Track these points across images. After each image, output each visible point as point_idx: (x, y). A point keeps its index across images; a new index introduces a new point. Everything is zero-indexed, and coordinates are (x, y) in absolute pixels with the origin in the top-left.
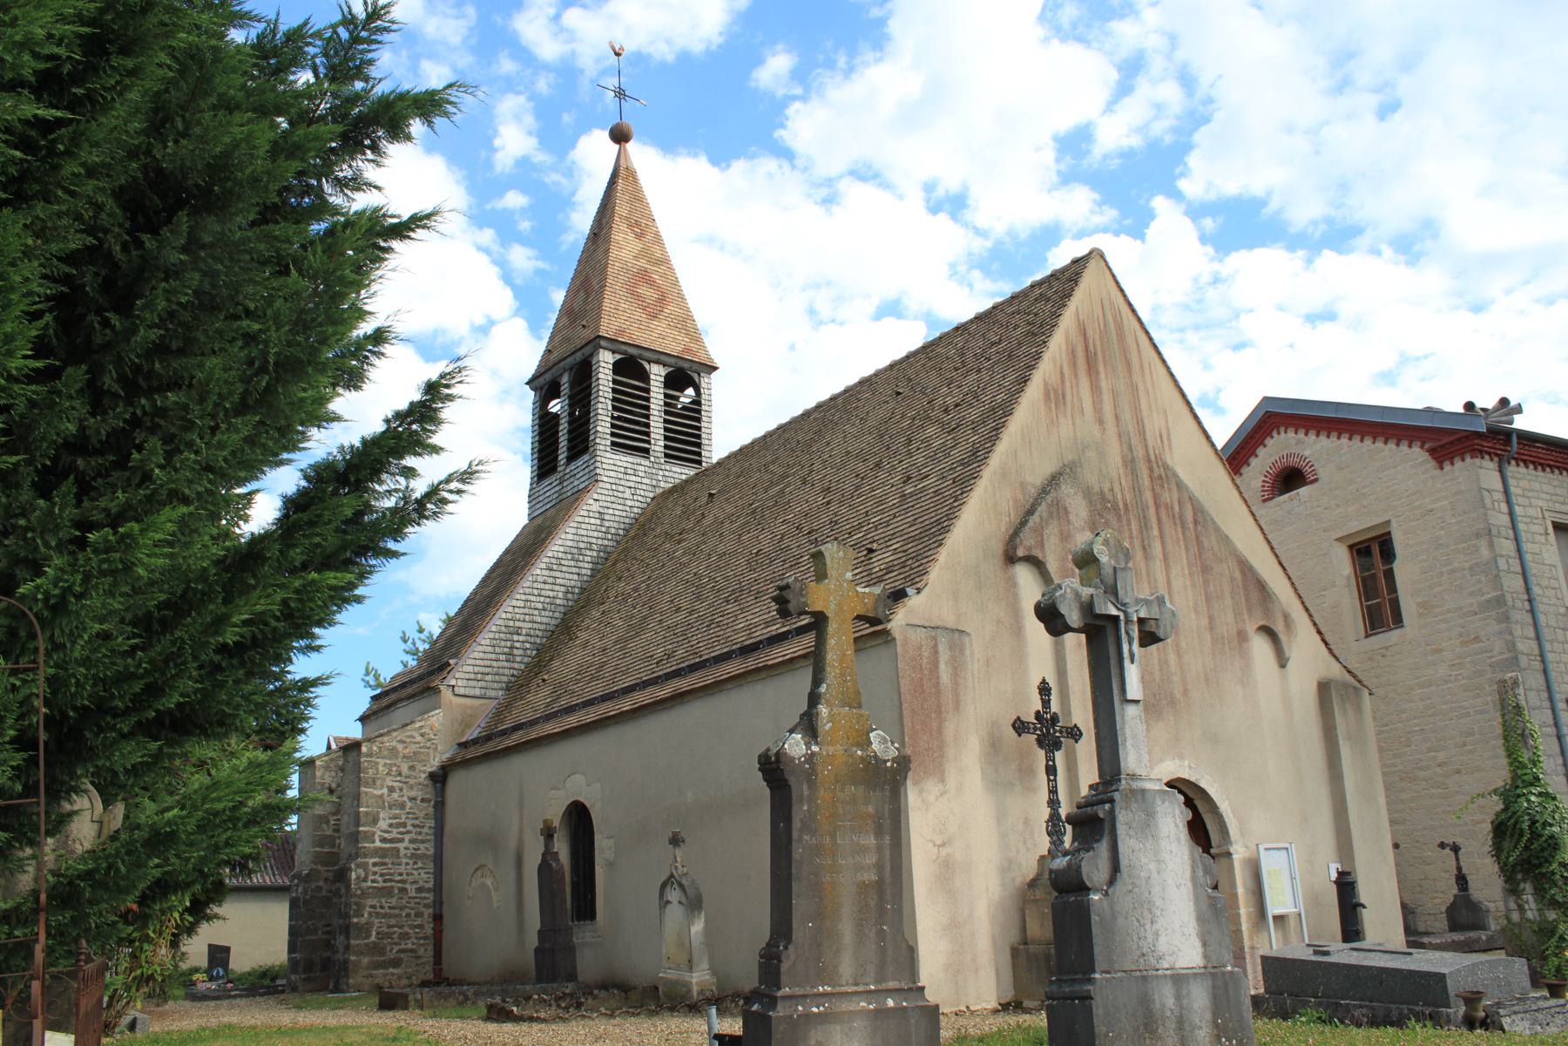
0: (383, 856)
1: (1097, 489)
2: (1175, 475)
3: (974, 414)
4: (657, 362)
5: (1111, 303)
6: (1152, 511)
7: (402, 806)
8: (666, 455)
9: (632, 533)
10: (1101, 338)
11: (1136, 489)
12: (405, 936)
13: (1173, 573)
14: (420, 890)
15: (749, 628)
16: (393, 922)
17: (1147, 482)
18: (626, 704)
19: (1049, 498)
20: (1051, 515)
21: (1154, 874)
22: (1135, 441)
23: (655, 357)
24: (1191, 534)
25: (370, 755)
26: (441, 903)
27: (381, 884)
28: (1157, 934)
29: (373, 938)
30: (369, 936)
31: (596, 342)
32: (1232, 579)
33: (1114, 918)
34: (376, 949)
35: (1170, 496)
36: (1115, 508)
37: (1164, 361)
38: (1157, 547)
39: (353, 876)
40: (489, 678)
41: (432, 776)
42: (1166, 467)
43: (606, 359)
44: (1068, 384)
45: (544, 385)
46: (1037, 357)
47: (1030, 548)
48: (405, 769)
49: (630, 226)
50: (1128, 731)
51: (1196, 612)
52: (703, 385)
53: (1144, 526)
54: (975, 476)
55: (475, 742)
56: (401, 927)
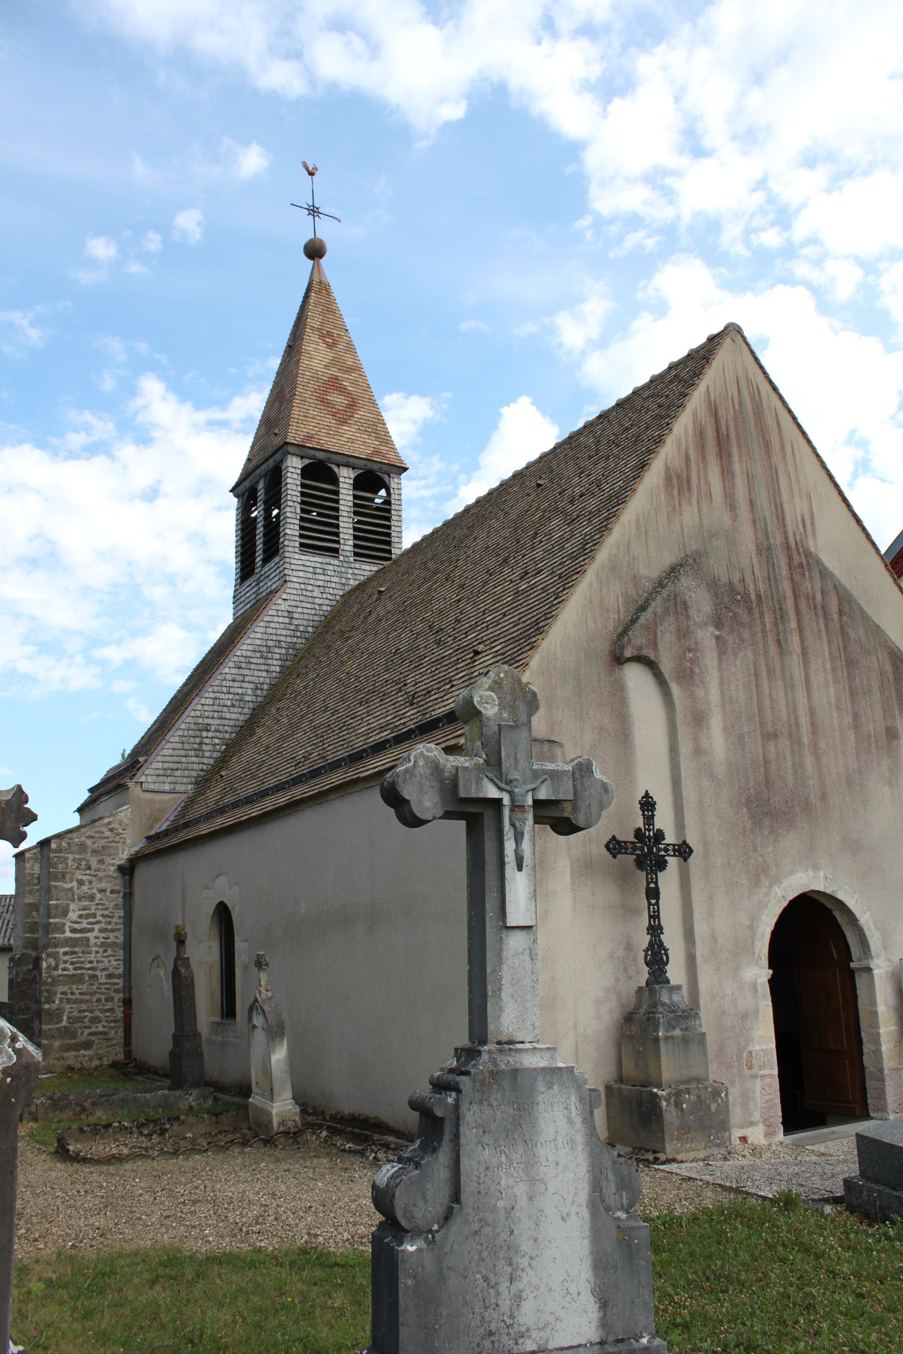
0: (74, 946)
1: (724, 580)
2: (819, 562)
3: (592, 504)
4: (347, 465)
5: (749, 381)
6: (790, 602)
7: (92, 898)
8: (356, 554)
9: (320, 630)
10: (735, 419)
11: (772, 578)
12: (96, 1020)
13: (813, 668)
14: (110, 976)
15: (367, 733)
16: (84, 1006)
17: (785, 572)
18: (255, 811)
19: (665, 592)
20: (667, 611)
21: (523, 1201)
22: (772, 526)
23: (345, 460)
24: (835, 625)
25: (59, 850)
26: (130, 989)
27: (72, 972)
28: (519, 1298)
29: (64, 1023)
30: (60, 1021)
31: (284, 449)
32: (882, 673)
33: (441, 1277)
34: (67, 1033)
35: (811, 585)
36: (746, 599)
37: (809, 442)
38: (795, 641)
39: (44, 965)
40: (178, 773)
41: (121, 868)
42: (808, 554)
43: (294, 466)
44: (694, 468)
45: (245, 492)
46: (659, 441)
47: (640, 648)
48: (94, 862)
49: (322, 337)
50: (506, 975)
51: (838, 708)
52: (393, 485)
53: (780, 616)
54: (580, 571)
55: (166, 833)
56: (91, 1012)
